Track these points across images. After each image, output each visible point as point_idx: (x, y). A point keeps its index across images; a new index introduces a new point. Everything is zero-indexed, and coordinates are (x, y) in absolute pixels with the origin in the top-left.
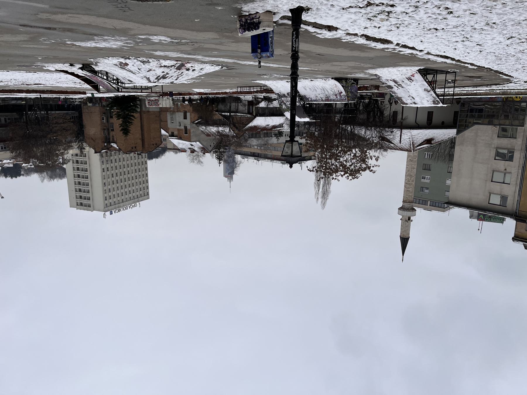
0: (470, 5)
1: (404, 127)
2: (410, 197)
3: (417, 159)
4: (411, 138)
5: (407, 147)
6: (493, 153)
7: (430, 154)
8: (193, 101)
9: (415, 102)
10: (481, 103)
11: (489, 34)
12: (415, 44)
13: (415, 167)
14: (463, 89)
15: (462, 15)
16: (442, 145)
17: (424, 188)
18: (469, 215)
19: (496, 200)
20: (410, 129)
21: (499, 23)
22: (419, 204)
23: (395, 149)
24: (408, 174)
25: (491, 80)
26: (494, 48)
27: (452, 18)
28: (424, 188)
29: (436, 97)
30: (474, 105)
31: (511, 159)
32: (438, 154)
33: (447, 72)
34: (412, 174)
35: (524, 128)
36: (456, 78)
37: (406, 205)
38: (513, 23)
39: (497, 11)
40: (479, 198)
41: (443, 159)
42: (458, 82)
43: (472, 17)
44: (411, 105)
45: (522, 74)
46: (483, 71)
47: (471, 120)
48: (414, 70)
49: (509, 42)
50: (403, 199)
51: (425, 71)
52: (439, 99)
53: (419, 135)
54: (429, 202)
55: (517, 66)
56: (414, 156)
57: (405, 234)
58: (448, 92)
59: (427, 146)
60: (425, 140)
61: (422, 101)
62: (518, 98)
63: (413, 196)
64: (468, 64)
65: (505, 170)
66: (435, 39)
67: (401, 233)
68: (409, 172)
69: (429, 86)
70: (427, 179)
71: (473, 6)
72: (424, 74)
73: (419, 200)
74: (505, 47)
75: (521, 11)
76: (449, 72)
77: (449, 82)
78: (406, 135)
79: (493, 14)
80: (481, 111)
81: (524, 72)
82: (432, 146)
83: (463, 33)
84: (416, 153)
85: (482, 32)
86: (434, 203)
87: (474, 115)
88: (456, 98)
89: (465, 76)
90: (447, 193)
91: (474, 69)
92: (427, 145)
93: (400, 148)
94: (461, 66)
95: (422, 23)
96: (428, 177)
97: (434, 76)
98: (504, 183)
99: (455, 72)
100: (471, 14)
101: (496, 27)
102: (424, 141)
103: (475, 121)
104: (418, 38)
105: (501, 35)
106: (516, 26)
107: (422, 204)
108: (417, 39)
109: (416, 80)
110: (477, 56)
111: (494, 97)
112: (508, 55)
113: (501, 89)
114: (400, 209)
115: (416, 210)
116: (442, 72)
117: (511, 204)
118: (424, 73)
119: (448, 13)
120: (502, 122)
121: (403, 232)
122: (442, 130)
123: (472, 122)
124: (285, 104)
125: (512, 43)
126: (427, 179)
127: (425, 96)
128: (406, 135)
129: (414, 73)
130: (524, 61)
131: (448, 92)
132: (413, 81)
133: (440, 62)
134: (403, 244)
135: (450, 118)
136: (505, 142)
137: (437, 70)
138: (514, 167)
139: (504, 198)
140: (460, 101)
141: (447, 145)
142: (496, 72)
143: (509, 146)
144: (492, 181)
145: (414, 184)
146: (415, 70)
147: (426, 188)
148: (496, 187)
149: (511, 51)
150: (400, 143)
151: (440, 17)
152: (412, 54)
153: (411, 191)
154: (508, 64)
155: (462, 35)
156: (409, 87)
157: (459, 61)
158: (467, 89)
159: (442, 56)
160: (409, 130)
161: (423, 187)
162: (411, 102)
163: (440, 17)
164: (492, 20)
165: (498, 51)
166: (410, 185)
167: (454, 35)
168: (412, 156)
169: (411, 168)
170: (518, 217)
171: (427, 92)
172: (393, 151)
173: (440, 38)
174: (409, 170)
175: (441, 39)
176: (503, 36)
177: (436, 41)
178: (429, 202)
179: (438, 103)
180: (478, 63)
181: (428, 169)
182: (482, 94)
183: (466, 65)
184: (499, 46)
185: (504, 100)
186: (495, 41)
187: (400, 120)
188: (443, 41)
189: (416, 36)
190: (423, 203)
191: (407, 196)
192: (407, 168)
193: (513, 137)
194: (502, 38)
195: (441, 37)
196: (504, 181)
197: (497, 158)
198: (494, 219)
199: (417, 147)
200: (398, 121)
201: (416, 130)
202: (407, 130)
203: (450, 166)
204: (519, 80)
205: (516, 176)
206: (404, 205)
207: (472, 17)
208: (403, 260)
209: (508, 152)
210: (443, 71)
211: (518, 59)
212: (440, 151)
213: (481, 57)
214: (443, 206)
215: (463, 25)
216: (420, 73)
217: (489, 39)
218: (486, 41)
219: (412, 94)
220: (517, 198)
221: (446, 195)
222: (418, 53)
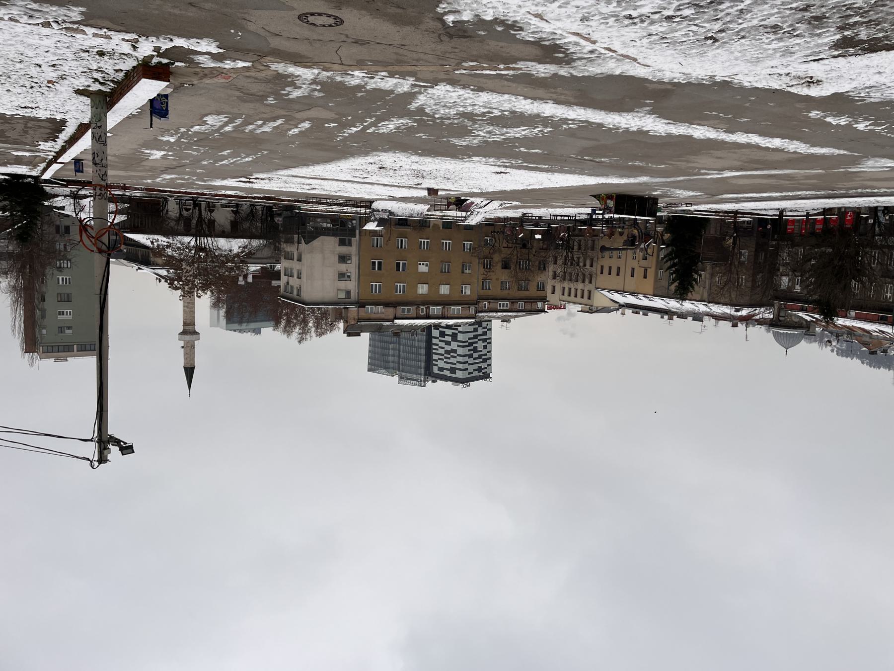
6: (337, 258)
22: (58, 352)
50: (184, 319)
54: (75, 346)
70: (67, 314)
73: (58, 346)
86: (83, 346)
107: (64, 352)
114: (180, 334)
124: (375, 216)
126: (67, 314)
136: (344, 250)
139: (348, 293)
178: (75, 346)
181: (66, 299)
193: (350, 244)
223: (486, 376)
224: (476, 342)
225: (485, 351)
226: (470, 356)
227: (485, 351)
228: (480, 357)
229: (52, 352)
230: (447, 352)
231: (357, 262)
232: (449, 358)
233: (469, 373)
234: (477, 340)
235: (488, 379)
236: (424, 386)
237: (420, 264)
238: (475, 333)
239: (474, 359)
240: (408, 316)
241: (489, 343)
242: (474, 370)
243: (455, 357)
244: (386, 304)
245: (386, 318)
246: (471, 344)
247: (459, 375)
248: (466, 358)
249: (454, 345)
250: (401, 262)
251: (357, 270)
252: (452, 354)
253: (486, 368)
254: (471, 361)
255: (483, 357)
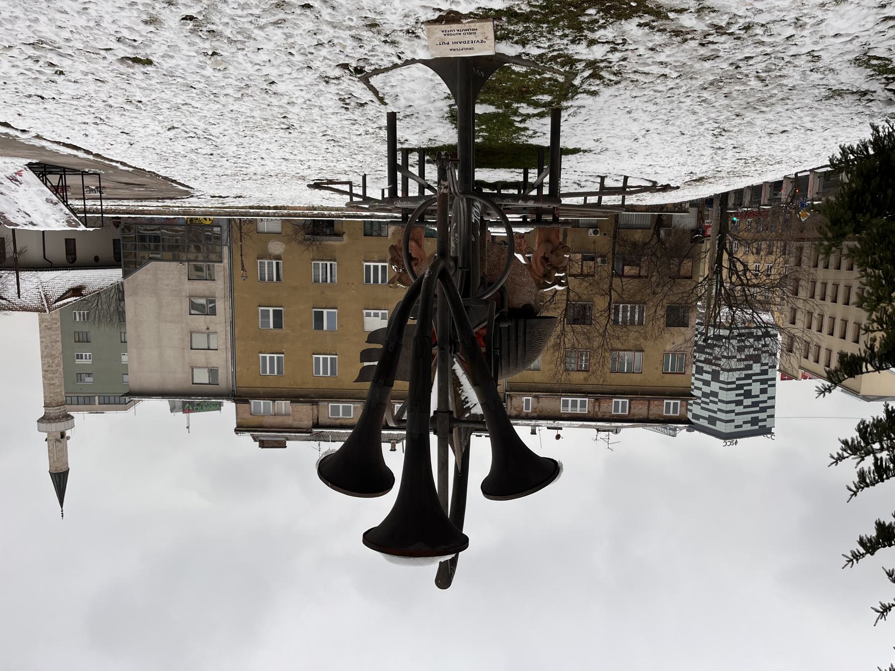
0: (92, 65)
1: (20, 267)
2: (56, 396)
3: (59, 324)
4: (40, 286)
5: (36, 303)
6: (186, 305)
7: (84, 313)
8: (482, 165)
9: (32, 222)
10: (154, 227)
11: (136, 118)
12: (8, 119)
13: (59, 339)
14: (120, 203)
15: (82, 81)
16: (103, 296)
17: (82, 375)
18: (169, 408)
19: (202, 377)
20: (36, 271)
21: (148, 103)
22: (78, 404)
23: (10, 309)
24: (45, 353)
25: (161, 191)
26: (151, 142)
27: (65, 82)
28: (82, 375)
29: (71, 214)
30: (145, 230)
31: (213, 312)
32: (97, 312)
33: (83, 172)
34: (53, 353)
35: (223, 264)
36: (102, 184)
37: (51, 412)
38: (168, 106)
39: (138, 82)
40: (177, 378)
41: (108, 320)
42: (107, 190)
43: (100, 87)
44: (26, 228)
45: (205, 185)
46: (144, 177)
47: (146, 254)
48: (19, 165)
49: (171, 134)
51: (42, 168)
52: (77, 217)
53: (56, 281)
54: (97, 398)
55: (194, 172)
56: (53, 319)
57: (58, 466)
58: (95, 207)
59: (75, 300)
60: (70, 290)
61: (46, 220)
62: (208, 220)
63: (63, 393)
64: (117, 162)
65: (208, 329)
66: (43, 114)
67: (50, 466)
68: (48, 349)
69: (55, 195)
70: (86, 358)
71: (97, 69)
72: (41, 173)
73: (78, 397)
74: (168, 140)
75: (175, 90)
76: (87, 173)
77: (92, 190)
78: (30, 281)
79: (134, 87)
80: (156, 239)
81: (206, 181)
82: (85, 299)
83: (92, 110)
84: (56, 314)
85: (124, 113)
86: (107, 399)
87: (148, 247)
88: (112, 218)
89: (117, 182)
90: (126, 378)
91: (128, 171)
92: (75, 298)
93: (20, 307)
94: (104, 165)
95: (10, 83)
96: (88, 354)
97: (61, 177)
98: (209, 349)
99: (99, 174)
100: (97, 81)
101: (145, 108)
102: (67, 292)
103: (151, 256)
104: (10, 108)
105: (155, 122)
106: (175, 112)
107: (85, 404)
108: (10, 109)
109: (28, 183)
110: (127, 151)
111: (172, 218)
112: (176, 154)
113: (180, 205)
114: (40, 421)
115: (73, 418)
116: (74, 172)
117: (225, 380)
118: (42, 170)
119: (56, 72)
120: (191, 256)
121: (54, 462)
122: (97, 270)
123: (147, 257)
125: (177, 136)
126: (86, 358)
127: (49, 212)
128: (30, 281)
129: (20, 169)
130: (202, 166)
131: (95, 207)
132: (21, 184)
133: (65, 154)
134: (57, 481)
135: (107, 252)
136: (200, 287)
137: (64, 168)
138: (220, 324)
139: (213, 372)
140: (120, 223)
141: (111, 295)
142: (166, 178)
143: (207, 293)
144: (191, 349)
145: (61, 369)
146: (22, 165)
147: (87, 375)
148: (200, 357)
149: (178, 147)
150: (19, 297)
151: (44, 78)
152: (6, 134)
153: (58, 384)
154: (179, 167)
155: (90, 112)
156: (14, 194)
157: (97, 155)
158: (126, 203)
159: (65, 145)
160: (34, 272)
161: (80, 374)
162: (24, 221)
163: (44, 78)
164: (135, 96)
165: (159, 147)
166: (53, 373)
167: (78, 112)
168: (49, 320)
169: (51, 342)
170: (237, 397)
171: (52, 204)
172: (6, 314)
173: (54, 114)
174: (46, 347)
175: (55, 116)
176: (160, 123)
177: (48, 117)
178: (97, 398)
179: (77, 225)
180: (133, 161)
181: (85, 340)
182: (152, 212)
183: (114, 164)
184: (158, 138)
185: (189, 223)
186: (149, 130)
187: (11, 254)
188: (61, 119)
189: (5, 104)
190: (86, 401)
191: (52, 395)
192: (42, 342)
194: (158, 126)
195: (54, 111)
196: (209, 347)
197: (193, 312)
198: (206, 406)
199: (55, 303)
200: (7, 256)
201: (47, 272)
202: (29, 272)
203: (123, 330)
204: (203, 193)
205: (224, 337)
206: (47, 411)
207: (100, 87)
208: (64, 515)
209: (207, 301)
210: (75, 170)
211: (192, 162)
212: (100, 307)
213: (134, 153)
214: (117, 401)
215: (87, 97)
216: (32, 171)
217: (139, 125)
218: (135, 129)
219: (23, 206)
220: (230, 369)
221: (124, 381)
222: (18, 134)
223: (766, 431)
224: (750, 384)
225: (763, 397)
226: (739, 403)
227: (763, 397)
228: (755, 404)
229: (71, 404)
230: (705, 395)
231: (229, 311)
232: (707, 404)
233: (736, 427)
234: (750, 381)
235: (769, 436)
236: (674, 436)
237: (368, 315)
238: (750, 372)
239: (745, 407)
240: (344, 422)
241: (770, 386)
242: (745, 423)
243: (716, 403)
244: (295, 397)
245: (296, 424)
246: (740, 387)
247: (720, 427)
248: (732, 407)
249: (715, 386)
250: (325, 311)
251: (229, 328)
252: (711, 398)
253: (764, 420)
254: (740, 409)
255: (761, 405)
